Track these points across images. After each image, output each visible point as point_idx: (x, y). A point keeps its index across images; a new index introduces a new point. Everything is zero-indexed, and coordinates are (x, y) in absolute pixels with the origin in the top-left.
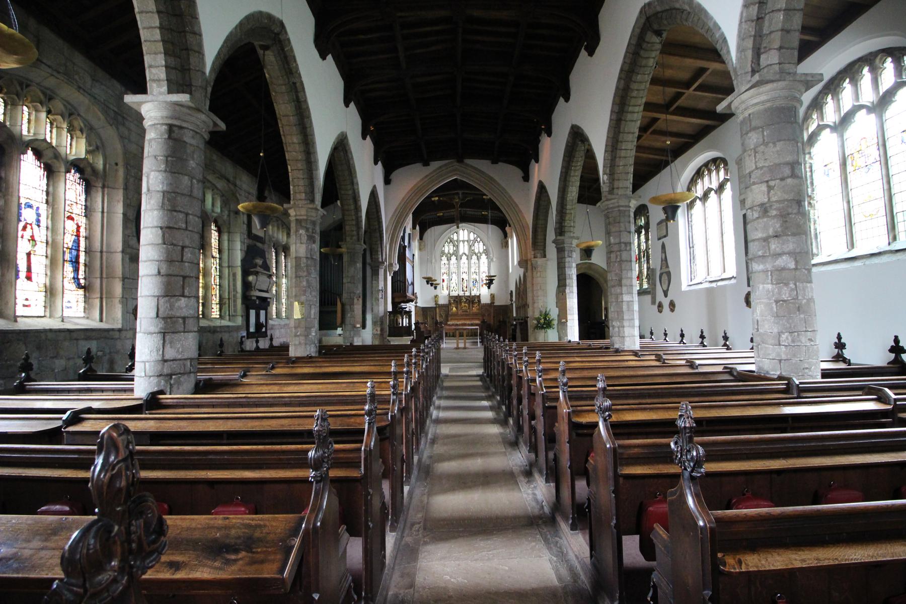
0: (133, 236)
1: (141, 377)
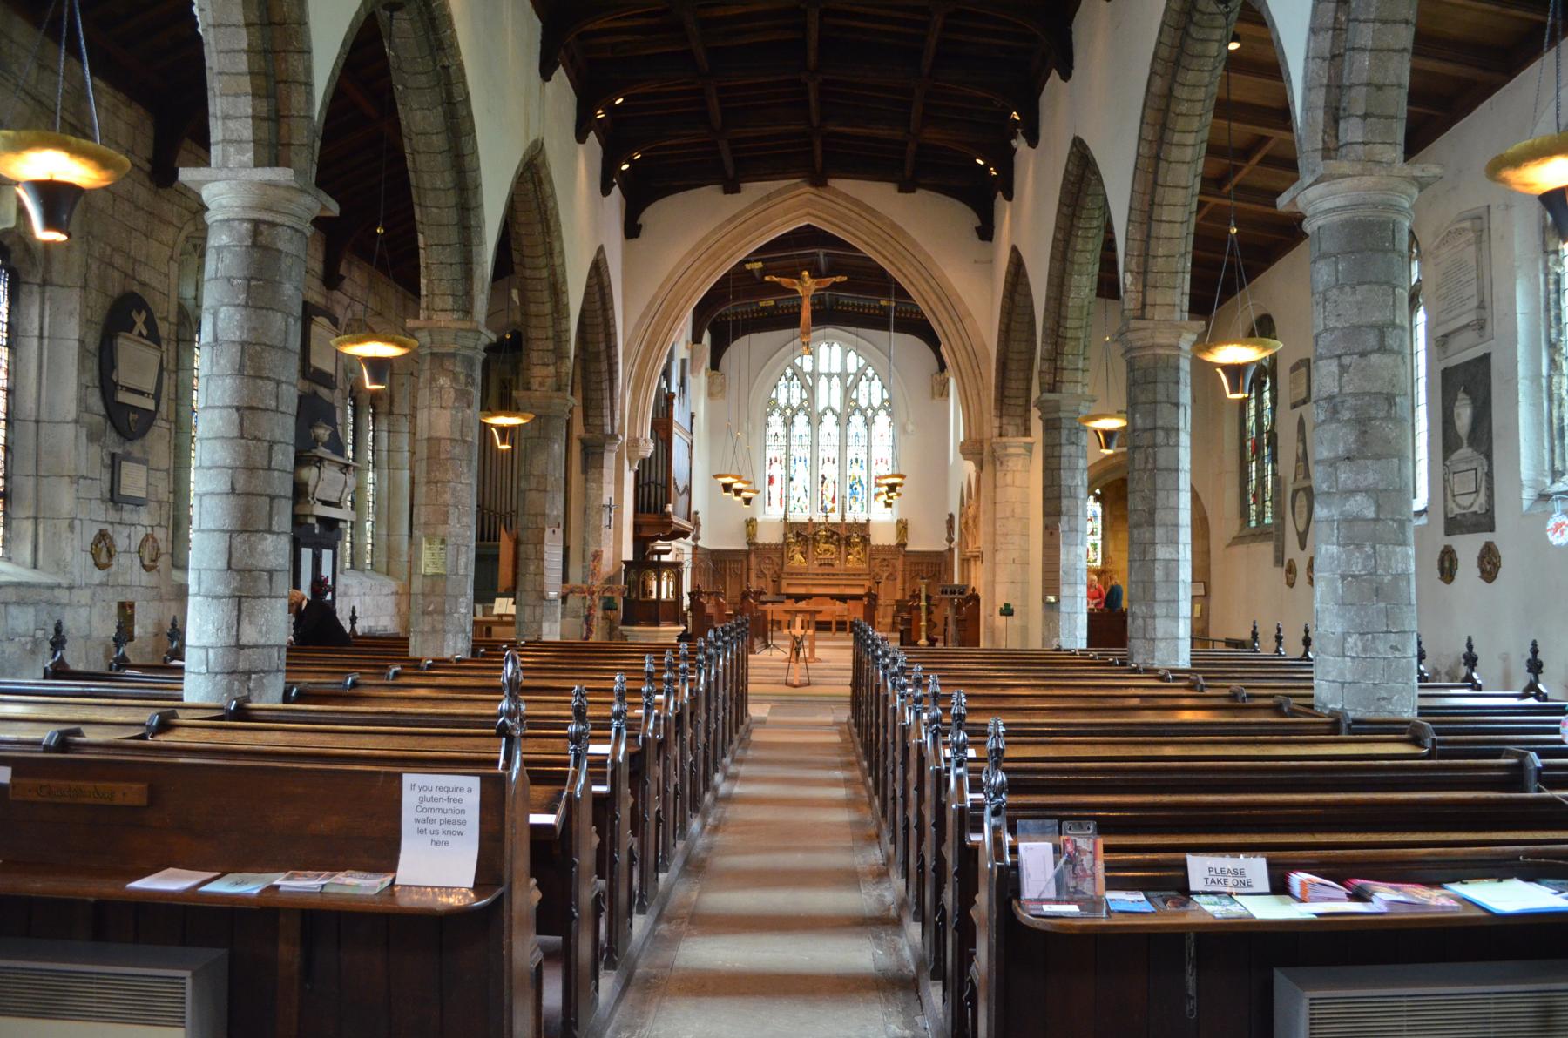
0: (95, 387)
1: (199, 673)
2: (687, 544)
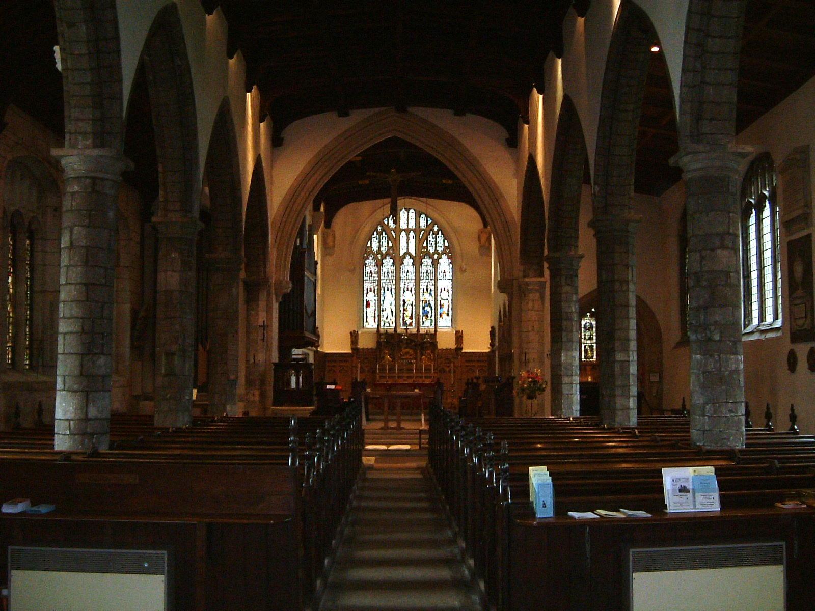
1: (65, 435)
2: (311, 350)
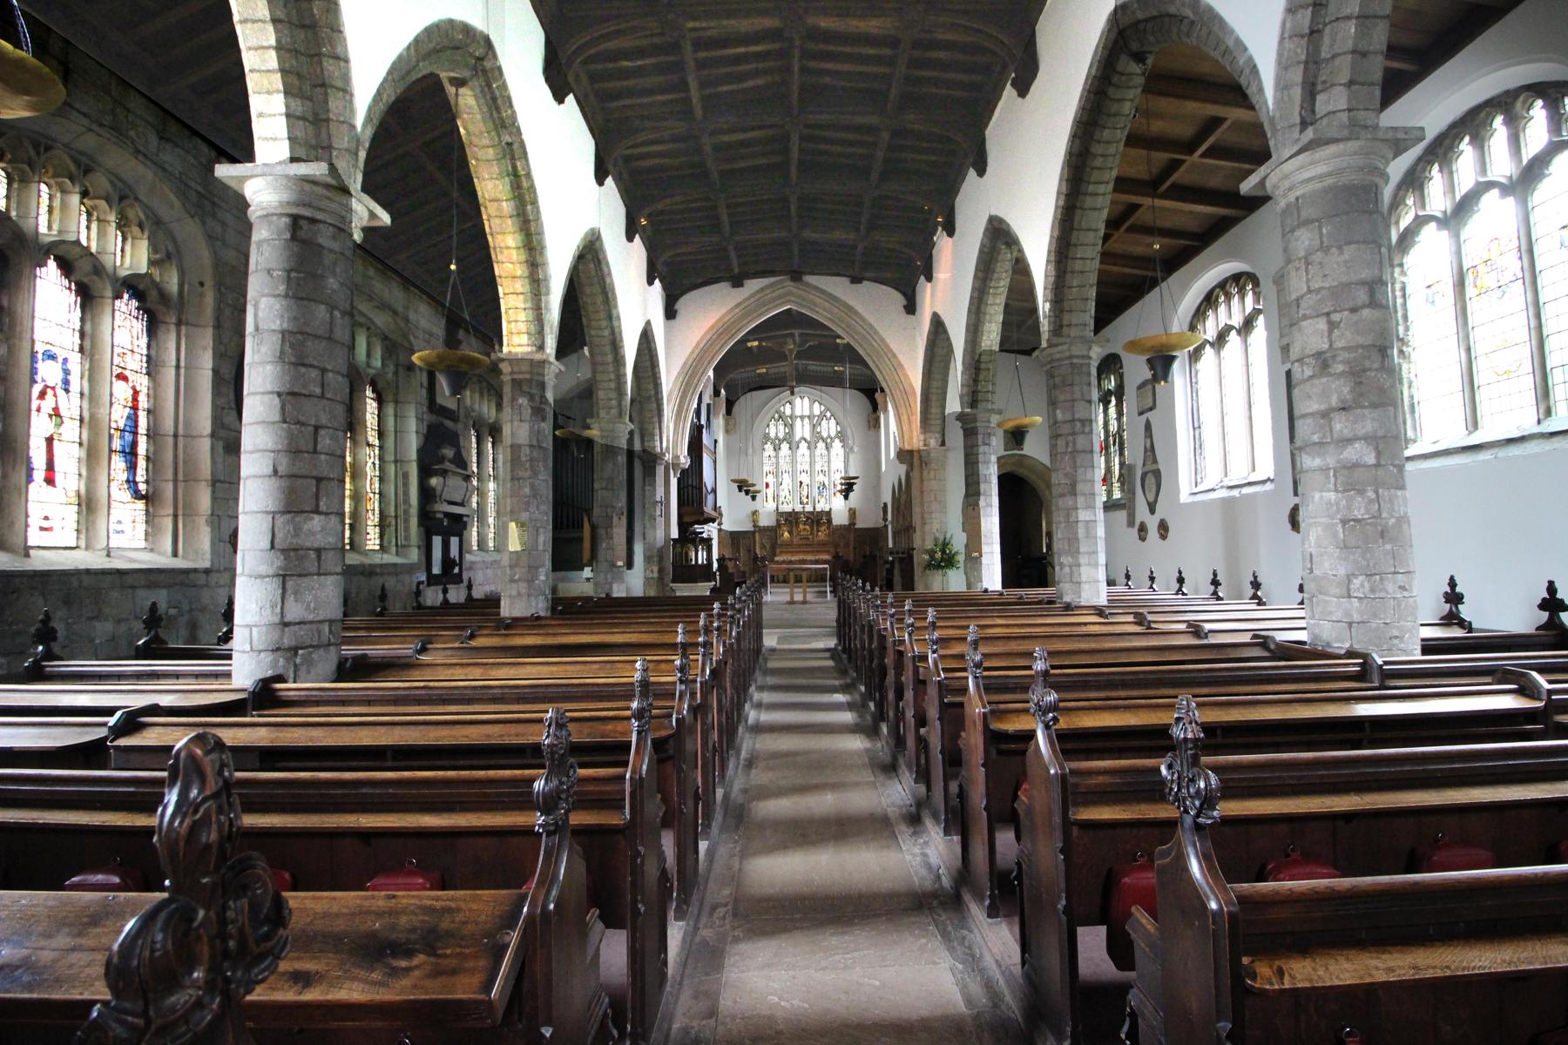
1: (243, 652)
